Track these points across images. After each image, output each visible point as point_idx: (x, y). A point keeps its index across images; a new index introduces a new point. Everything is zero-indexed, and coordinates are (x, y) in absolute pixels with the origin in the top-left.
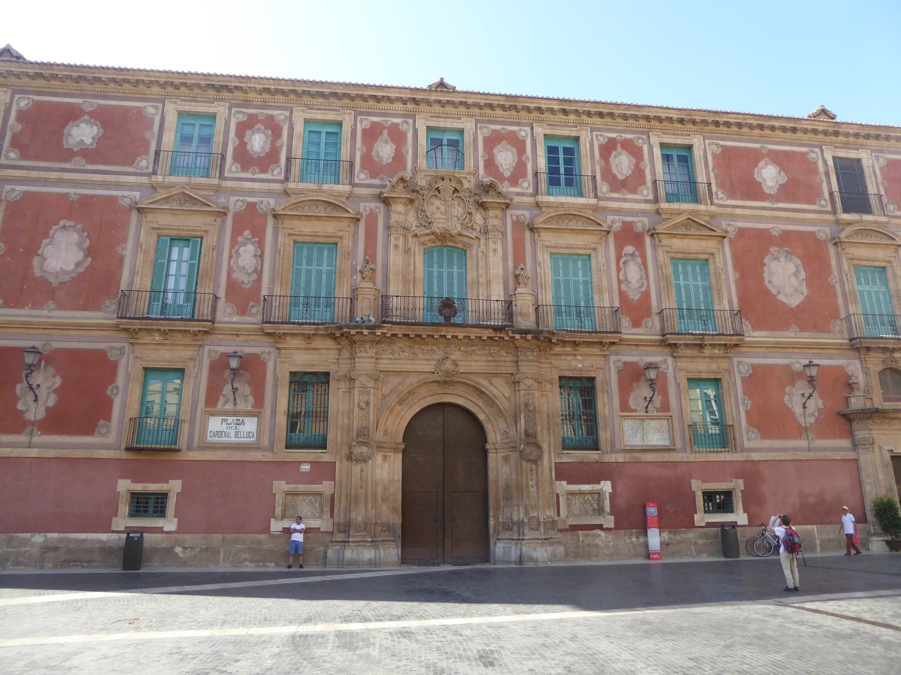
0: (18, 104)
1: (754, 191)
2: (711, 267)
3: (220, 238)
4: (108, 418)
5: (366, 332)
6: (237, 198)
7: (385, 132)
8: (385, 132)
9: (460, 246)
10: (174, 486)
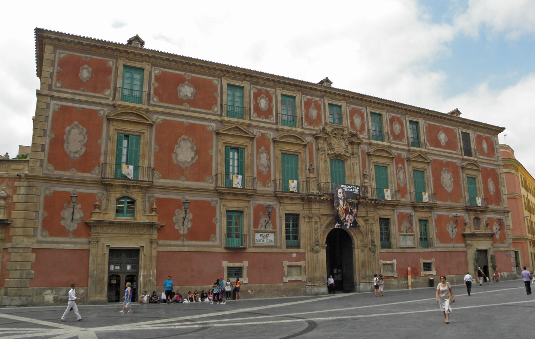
0: (155, 72)
1: (437, 144)
2: (425, 175)
3: (253, 150)
4: (215, 233)
5: (318, 198)
7: (313, 104)
8: (313, 104)
9: (343, 159)
10: (245, 264)
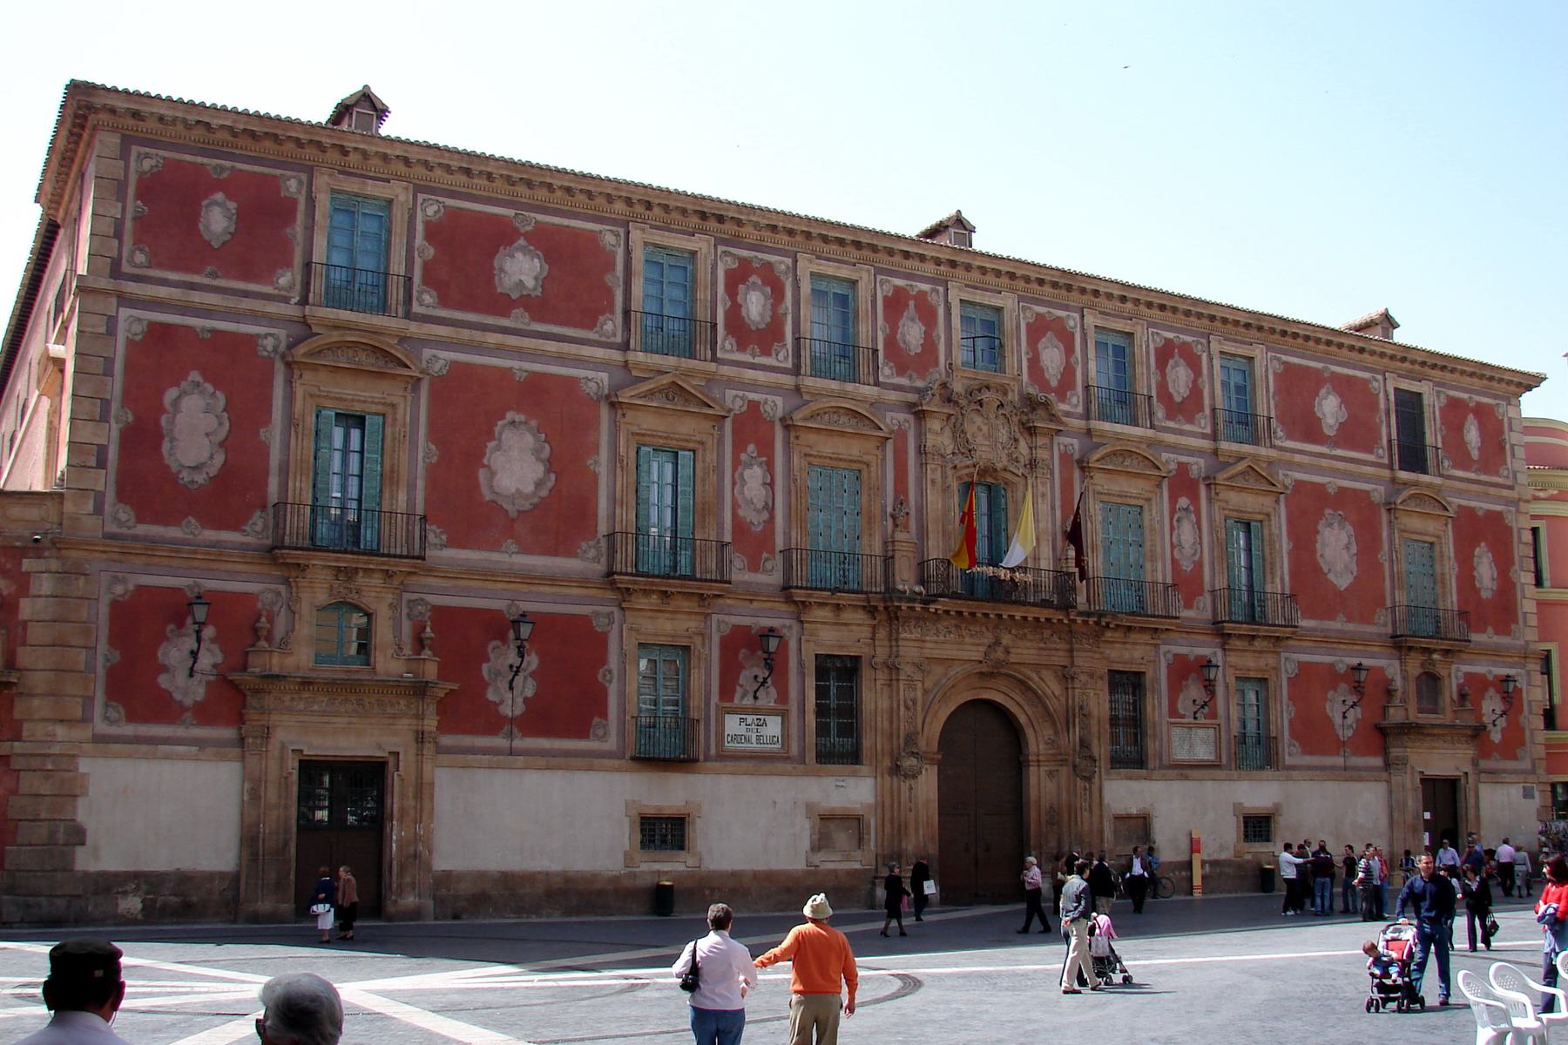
0: (424, 210)
1: (1309, 429)
3: (720, 456)
4: (604, 714)
6: (734, 392)
7: (912, 303)
